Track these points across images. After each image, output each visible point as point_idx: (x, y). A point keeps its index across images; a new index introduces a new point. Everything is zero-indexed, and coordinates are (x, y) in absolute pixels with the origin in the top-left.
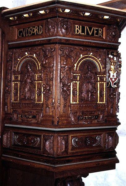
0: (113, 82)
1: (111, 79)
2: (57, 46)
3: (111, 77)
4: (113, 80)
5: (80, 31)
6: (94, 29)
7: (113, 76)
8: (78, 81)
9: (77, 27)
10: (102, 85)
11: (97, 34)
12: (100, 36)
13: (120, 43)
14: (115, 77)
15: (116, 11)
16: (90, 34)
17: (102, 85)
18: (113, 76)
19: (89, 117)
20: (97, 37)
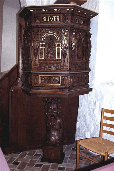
0: (64, 47)
1: (63, 45)
2: (76, 164)
3: (63, 44)
4: (65, 45)
5: (45, 20)
6: (54, 17)
7: (65, 43)
8: (44, 47)
9: (44, 18)
10: (59, 49)
11: (56, 20)
12: (58, 20)
13: (91, 28)
14: (66, 44)
15: (65, 5)
16: (52, 20)
17: (59, 49)
18: (65, 43)
19: (51, 67)
20: (56, 22)
